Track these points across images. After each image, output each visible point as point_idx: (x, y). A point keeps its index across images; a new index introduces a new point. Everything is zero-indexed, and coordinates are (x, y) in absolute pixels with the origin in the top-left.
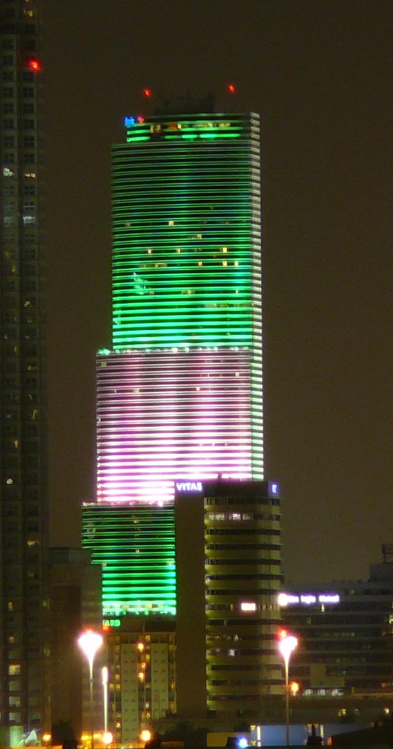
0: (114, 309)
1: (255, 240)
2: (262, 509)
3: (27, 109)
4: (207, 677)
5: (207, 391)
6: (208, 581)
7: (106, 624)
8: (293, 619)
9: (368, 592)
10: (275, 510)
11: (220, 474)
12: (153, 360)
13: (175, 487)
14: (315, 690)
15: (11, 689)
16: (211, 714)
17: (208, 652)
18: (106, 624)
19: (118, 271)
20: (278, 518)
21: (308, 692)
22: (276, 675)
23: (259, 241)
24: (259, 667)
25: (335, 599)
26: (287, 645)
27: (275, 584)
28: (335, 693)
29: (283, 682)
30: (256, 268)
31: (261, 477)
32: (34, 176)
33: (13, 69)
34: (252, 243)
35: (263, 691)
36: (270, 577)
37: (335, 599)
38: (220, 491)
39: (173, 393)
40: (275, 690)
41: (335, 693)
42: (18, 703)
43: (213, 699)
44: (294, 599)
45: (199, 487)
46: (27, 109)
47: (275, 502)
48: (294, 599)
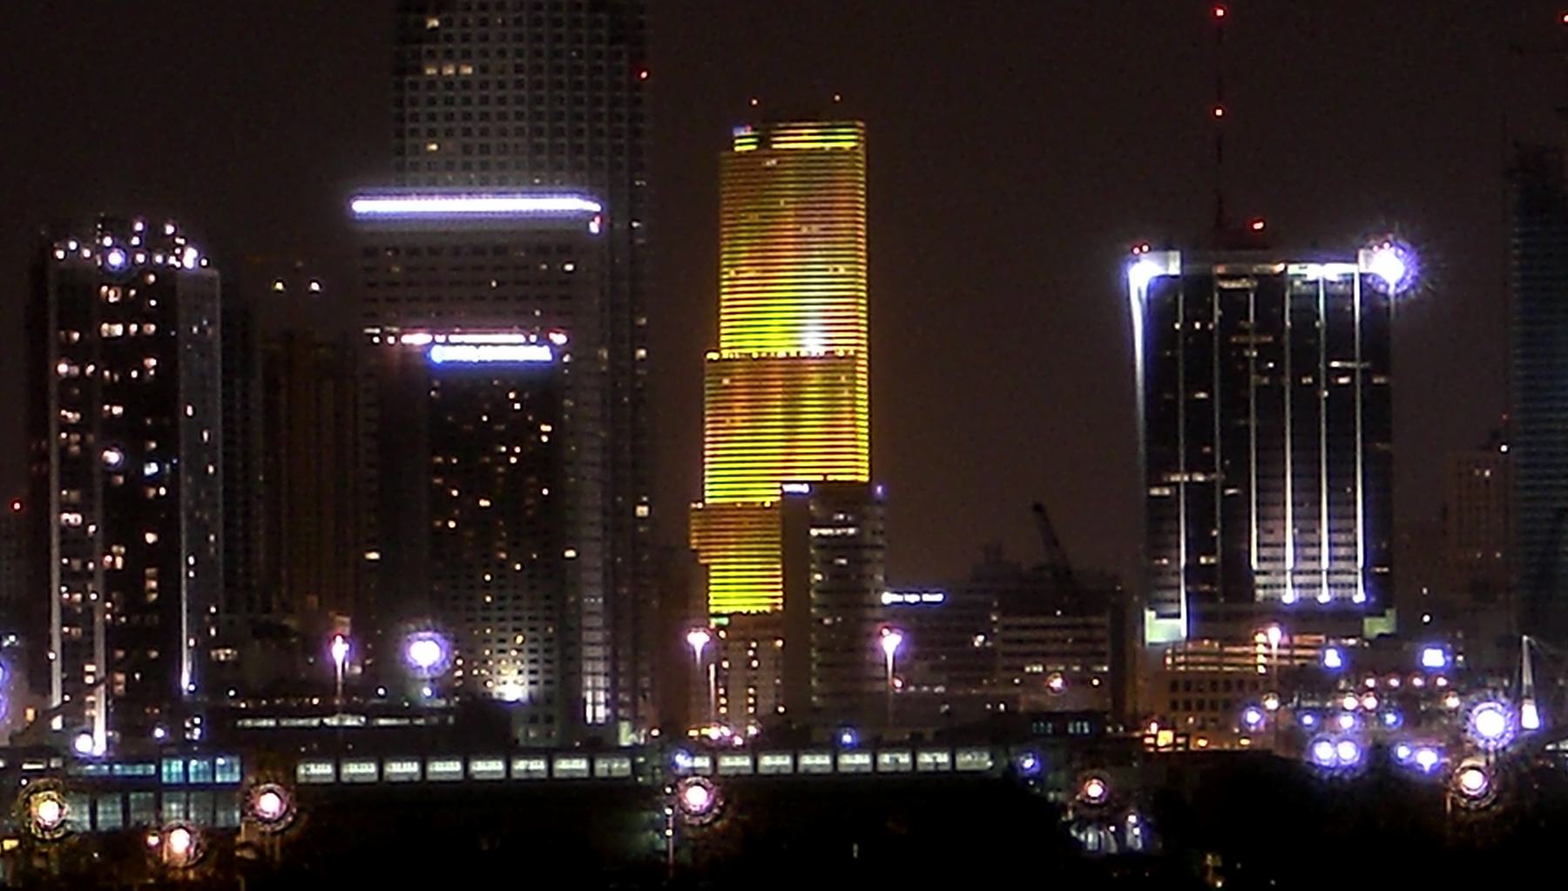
0: (723, 240)
1: (860, 240)
2: (867, 509)
3: (637, 133)
4: (812, 659)
5: (813, 399)
6: (813, 551)
7: (714, 622)
8: (899, 616)
9: (969, 592)
10: (879, 511)
11: (825, 475)
12: (759, 367)
13: (781, 488)
14: (917, 686)
15: (621, 669)
16: (817, 710)
17: (813, 649)
18: (714, 622)
19: (727, 222)
20: (882, 533)
21: (912, 689)
22: (880, 673)
23: (864, 322)
24: (868, 591)
25: (939, 598)
26: (891, 643)
27: (880, 625)
28: (938, 689)
29: (886, 679)
30: (860, 240)
31: (865, 479)
32: (644, 183)
33: (624, 79)
34: (858, 202)
35: (867, 687)
36: (878, 620)
37: (939, 598)
38: (831, 494)
39: (780, 383)
40: (880, 686)
41: (938, 689)
42: (627, 699)
43: (818, 606)
44: (898, 598)
45: (805, 488)
46: (637, 133)
47: (879, 503)
48: (898, 598)
